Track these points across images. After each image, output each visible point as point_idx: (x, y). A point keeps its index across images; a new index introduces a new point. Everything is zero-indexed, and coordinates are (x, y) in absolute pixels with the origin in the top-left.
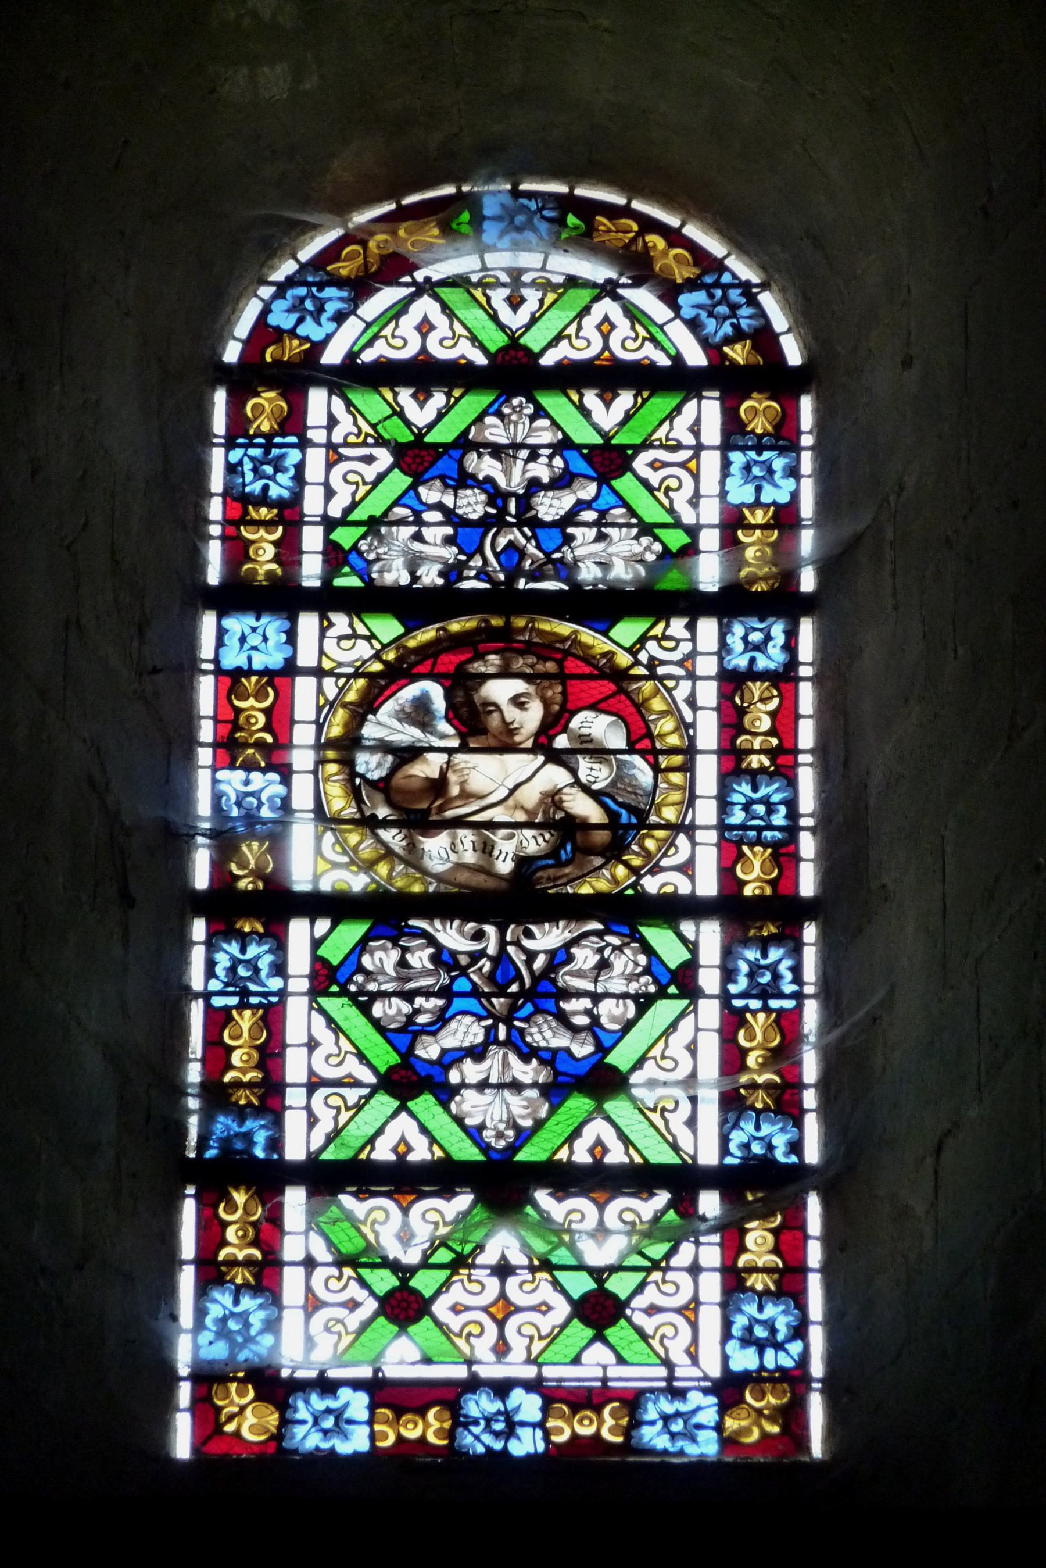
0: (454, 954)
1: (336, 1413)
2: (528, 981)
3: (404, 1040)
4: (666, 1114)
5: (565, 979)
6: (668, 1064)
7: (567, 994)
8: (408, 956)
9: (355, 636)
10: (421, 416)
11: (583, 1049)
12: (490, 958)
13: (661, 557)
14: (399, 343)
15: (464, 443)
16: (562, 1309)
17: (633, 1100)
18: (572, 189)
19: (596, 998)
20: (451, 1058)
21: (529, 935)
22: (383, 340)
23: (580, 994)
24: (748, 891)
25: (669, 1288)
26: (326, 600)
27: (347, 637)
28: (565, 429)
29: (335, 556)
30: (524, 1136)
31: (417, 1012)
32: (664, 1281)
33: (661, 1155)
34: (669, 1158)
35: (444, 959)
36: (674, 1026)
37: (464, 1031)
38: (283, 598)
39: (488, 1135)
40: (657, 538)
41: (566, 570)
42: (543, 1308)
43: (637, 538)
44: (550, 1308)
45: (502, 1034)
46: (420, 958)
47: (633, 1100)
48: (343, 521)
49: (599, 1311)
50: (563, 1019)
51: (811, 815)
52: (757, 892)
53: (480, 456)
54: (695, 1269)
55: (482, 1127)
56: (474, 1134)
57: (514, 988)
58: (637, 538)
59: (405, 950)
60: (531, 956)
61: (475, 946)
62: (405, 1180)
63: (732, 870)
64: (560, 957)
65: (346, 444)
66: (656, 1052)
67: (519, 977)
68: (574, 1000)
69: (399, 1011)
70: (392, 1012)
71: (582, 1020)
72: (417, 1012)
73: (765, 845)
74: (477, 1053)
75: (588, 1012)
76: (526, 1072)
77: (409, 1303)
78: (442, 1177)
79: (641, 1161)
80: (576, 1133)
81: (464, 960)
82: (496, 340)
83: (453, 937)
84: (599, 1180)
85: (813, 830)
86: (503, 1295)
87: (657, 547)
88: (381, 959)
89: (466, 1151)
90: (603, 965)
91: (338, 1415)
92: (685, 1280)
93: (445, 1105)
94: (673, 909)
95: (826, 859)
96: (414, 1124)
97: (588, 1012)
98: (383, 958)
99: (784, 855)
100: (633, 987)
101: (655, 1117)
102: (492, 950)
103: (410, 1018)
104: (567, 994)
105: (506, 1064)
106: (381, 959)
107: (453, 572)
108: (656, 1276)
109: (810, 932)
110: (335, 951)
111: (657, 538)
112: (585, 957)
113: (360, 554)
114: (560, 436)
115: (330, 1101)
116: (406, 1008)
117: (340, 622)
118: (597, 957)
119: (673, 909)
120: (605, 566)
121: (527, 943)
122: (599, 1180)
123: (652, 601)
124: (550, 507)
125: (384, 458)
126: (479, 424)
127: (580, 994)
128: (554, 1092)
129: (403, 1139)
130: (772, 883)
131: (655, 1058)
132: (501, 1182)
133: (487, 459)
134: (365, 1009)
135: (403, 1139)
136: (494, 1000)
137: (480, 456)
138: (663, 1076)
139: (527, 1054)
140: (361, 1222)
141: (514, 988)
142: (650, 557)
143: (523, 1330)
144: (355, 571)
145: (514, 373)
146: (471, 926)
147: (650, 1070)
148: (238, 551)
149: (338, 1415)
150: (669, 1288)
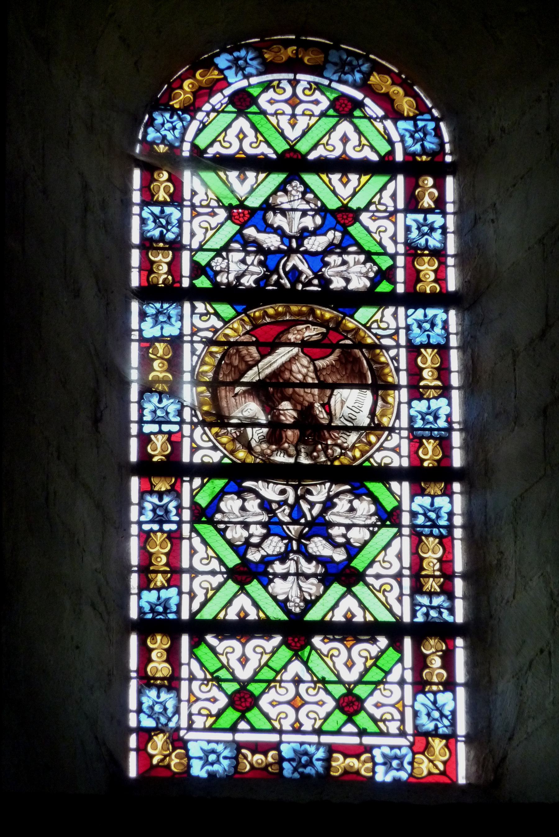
0: (270, 502)
1: (208, 763)
2: (309, 518)
3: (242, 550)
4: (386, 593)
5: (330, 517)
6: (387, 565)
7: (332, 525)
8: (246, 504)
9: (208, 313)
10: (242, 190)
11: (339, 556)
12: (289, 505)
13: (377, 273)
14: (227, 145)
15: (268, 206)
16: (331, 704)
17: (367, 585)
18: (432, 108)
19: (349, 527)
20: (267, 561)
21: (311, 493)
22: (218, 143)
23: (339, 525)
24: (426, 464)
25: (387, 693)
26: (194, 294)
27: (206, 315)
28: (323, 200)
29: (198, 270)
30: (309, 604)
31: (251, 536)
32: (385, 689)
33: (384, 617)
34: (390, 618)
35: (266, 505)
36: (388, 545)
37: (275, 545)
38: (173, 294)
39: (290, 605)
40: (375, 264)
41: (325, 282)
42: (321, 703)
43: (364, 263)
44: (324, 703)
45: (295, 547)
46: (253, 504)
47: (367, 585)
48: (201, 248)
49: (350, 705)
50: (329, 539)
51: (459, 423)
52: (431, 465)
53: (275, 214)
54: (402, 683)
55: (287, 600)
56: (283, 604)
57: (303, 521)
58: (364, 263)
59: (244, 500)
60: (312, 505)
61: (281, 498)
62: (243, 629)
63: (417, 452)
64: (329, 504)
65: (201, 206)
66: (380, 558)
67: (304, 516)
68: (337, 528)
69: (242, 536)
70: (236, 536)
71: (341, 540)
72: (251, 536)
73: (435, 439)
74: (283, 558)
75: (344, 536)
76: (309, 568)
77: (243, 697)
78: (264, 628)
79: (372, 619)
80: (336, 605)
81: (274, 506)
82: (281, 146)
83: (270, 491)
84: (349, 631)
85: (460, 430)
86: (298, 694)
87: (375, 268)
88: (231, 506)
89: (276, 613)
90: (352, 509)
91: (207, 763)
92: (396, 689)
93: (265, 587)
94: (385, 474)
95: (466, 447)
96: (249, 601)
97: (344, 536)
98: (231, 504)
99: (445, 443)
100: (369, 522)
101: (380, 595)
102: (291, 501)
103: (247, 540)
104: (332, 525)
105: (290, 224)
106: (231, 506)
107: (263, 280)
108: (381, 687)
109: (457, 487)
110: (203, 500)
111: (375, 264)
112: (342, 504)
113: (211, 268)
114: (319, 204)
115: (203, 585)
116: (245, 534)
117: (200, 307)
118: (349, 505)
119: (385, 474)
120: (348, 280)
121: (309, 497)
122: (349, 631)
123: (369, 297)
124: (316, 244)
125: (222, 214)
126: (274, 196)
127: (339, 525)
128: (326, 580)
129: (242, 609)
130: (438, 461)
131: (379, 561)
132: (297, 631)
133: (279, 215)
134: (222, 533)
135: (242, 609)
136: (291, 527)
137: (275, 214)
138: (383, 572)
139: (309, 558)
140: (220, 654)
141: (303, 521)
142: (372, 275)
143: (285, 691)
144: (208, 277)
145: (292, 164)
146: (280, 487)
147: (376, 569)
148: (148, 267)
149: (207, 763)
150: (387, 693)
